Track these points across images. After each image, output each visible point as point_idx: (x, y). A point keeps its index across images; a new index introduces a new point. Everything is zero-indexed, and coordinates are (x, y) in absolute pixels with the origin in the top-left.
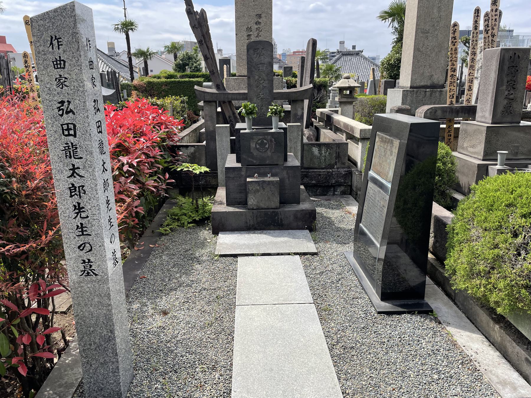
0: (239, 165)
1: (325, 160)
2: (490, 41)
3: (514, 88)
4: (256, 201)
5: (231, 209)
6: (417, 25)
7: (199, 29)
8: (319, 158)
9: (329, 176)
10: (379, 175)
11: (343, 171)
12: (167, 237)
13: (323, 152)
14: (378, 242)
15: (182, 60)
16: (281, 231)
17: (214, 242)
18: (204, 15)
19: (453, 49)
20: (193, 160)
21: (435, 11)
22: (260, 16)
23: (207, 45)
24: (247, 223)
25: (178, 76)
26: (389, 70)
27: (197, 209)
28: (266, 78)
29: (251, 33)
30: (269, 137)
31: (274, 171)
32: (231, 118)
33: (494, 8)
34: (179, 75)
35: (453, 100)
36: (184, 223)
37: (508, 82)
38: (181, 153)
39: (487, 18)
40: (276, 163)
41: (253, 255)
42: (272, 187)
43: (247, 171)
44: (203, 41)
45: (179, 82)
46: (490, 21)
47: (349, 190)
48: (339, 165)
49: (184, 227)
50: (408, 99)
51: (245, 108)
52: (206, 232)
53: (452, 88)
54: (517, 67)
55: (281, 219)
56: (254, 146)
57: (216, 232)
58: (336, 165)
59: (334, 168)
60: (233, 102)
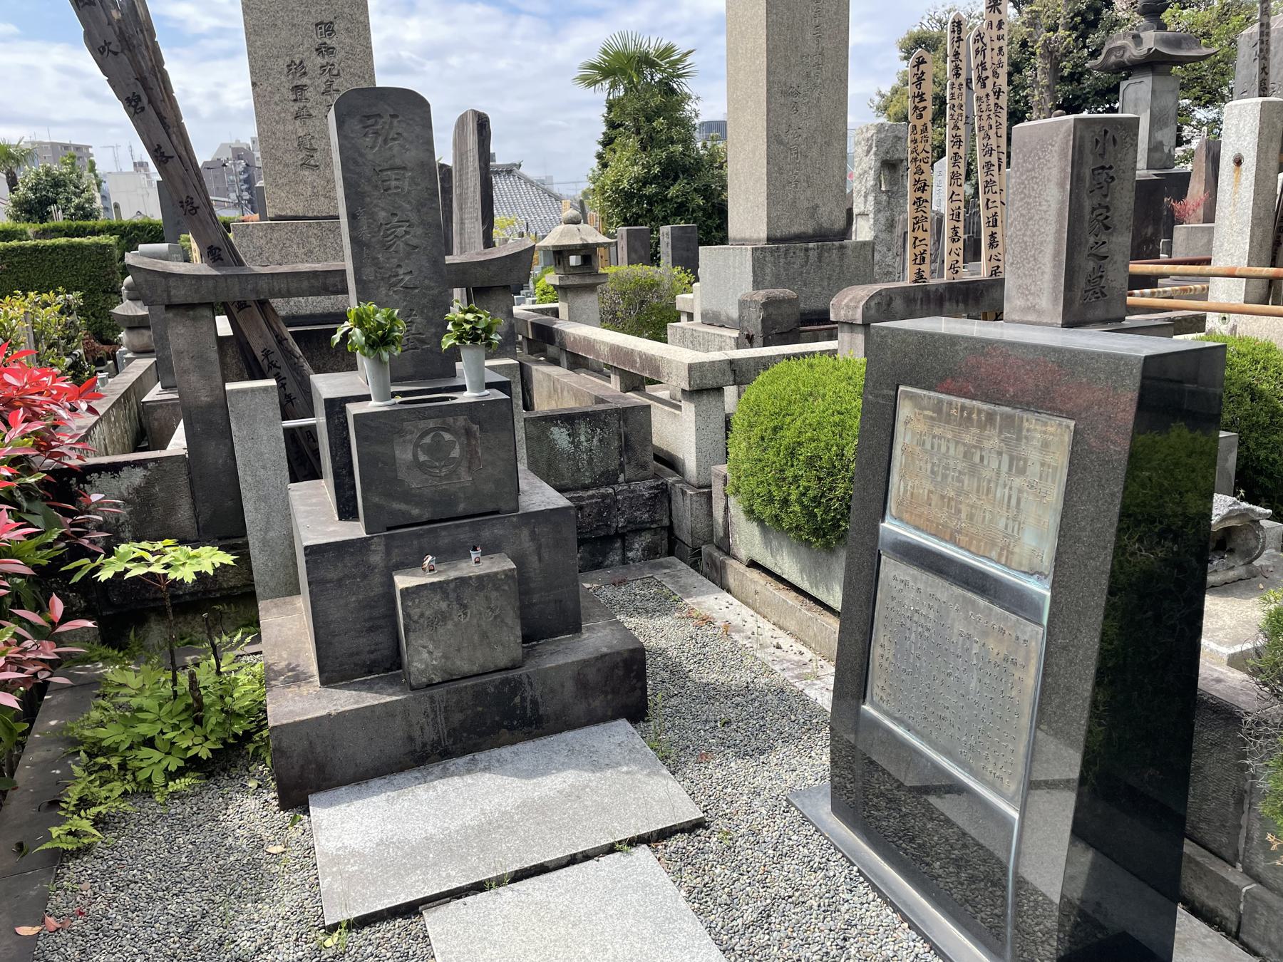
0: (356, 530)
1: (590, 460)
2: (992, 107)
3: (1107, 228)
4: (438, 654)
5: (345, 700)
6: (770, 72)
7: (124, 58)
8: (572, 458)
9: (608, 508)
10: (953, 541)
11: (644, 488)
12: (88, 865)
13: (583, 438)
14: (1010, 800)
15: (34, 189)
16: (539, 742)
17: (297, 851)
18: (140, 10)
19: (919, 128)
20: (147, 522)
21: (809, 36)
22: (329, 28)
23: (158, 114)
24: (411, 739)
25: (30, 231)
26: (618, 206)
27: (196, 714)
28: (414, 217)
29: (305, 81)
30: (461, 421)
31: (486, 534)
32: (272, 358)
33: (995, 18)
34: (31, 228)
35: (922, 267)
36: (149, 780)
37: (1094, 209)
38: (95, 497)
39: (980, 45)
40: (490, 507)
41: (479, 887)
42: (494, 594)
43: (388, 552)
44: (145, 100)
45: (35, 249)
46: (988, 52)
47: (665, 542)
48: (630, 471)
49: (150, 794)
50: (768, 271)
51: (360, 322)
52: (251, 803)
53: (920, 234)
54: (1111, 168)
55: (534, 703)
56: (409, 456)
57: (295, 798)
58: (623, 471)
59: (616, 482)
60: (277, 303)
